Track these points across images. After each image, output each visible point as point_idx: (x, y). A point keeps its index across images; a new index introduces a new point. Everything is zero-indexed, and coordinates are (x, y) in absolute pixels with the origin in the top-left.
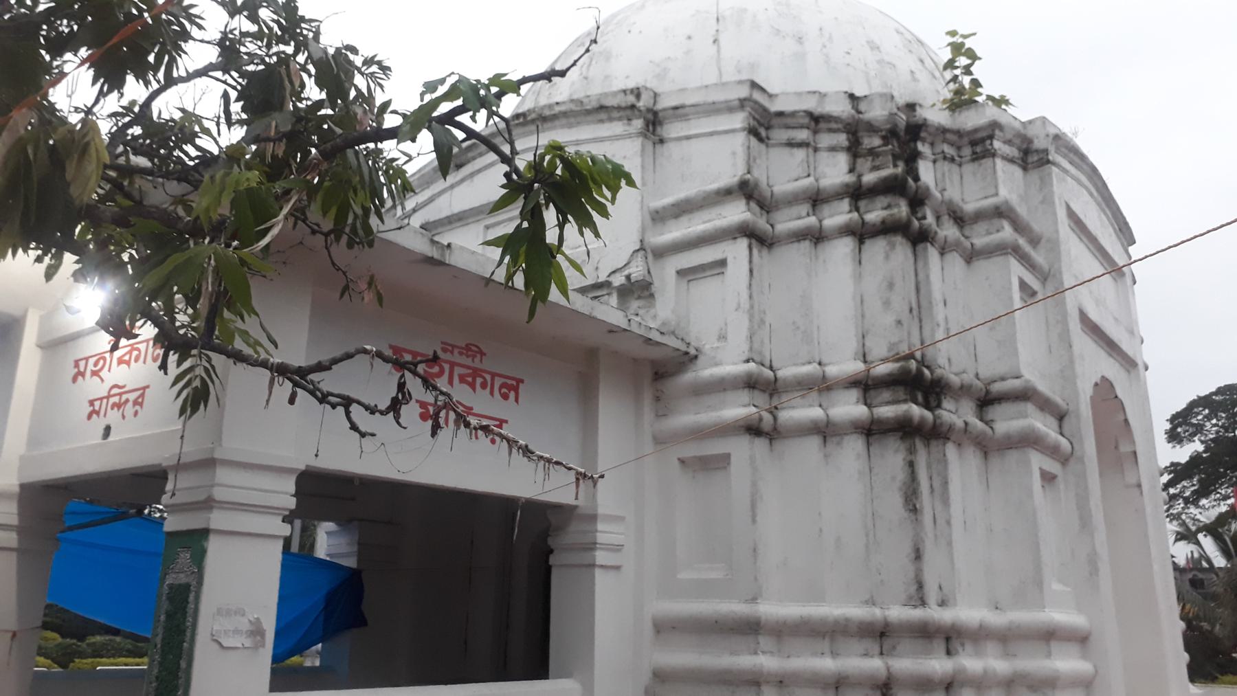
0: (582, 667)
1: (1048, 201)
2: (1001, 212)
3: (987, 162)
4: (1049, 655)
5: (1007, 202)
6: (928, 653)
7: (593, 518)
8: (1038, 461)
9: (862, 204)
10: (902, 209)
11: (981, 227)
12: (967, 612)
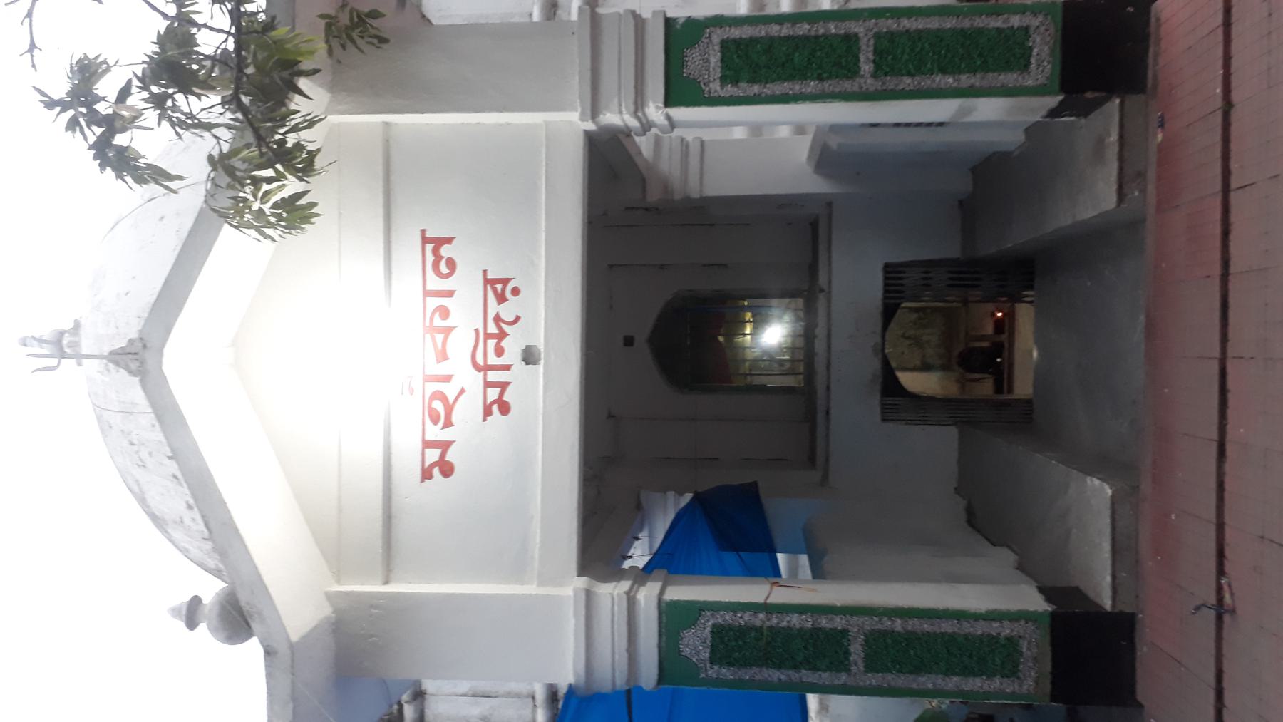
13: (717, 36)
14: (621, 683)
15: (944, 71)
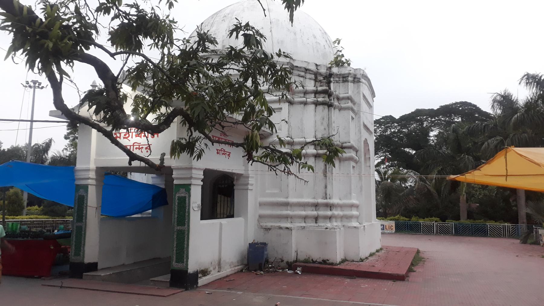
0: (244, 213)
1: (359, 93)
2: (349, 98)
3: (346, 83)
4: (351, 210)
5: (351, 96)
6: (327, 210)
7: (248, 177)
8: (353, 164)
9: (317, 95)
10: (327, 99)
11: (343, 101)
12: (335, 201)
13: (187, 196)
14: (76, 177)
15: (177, 244)
